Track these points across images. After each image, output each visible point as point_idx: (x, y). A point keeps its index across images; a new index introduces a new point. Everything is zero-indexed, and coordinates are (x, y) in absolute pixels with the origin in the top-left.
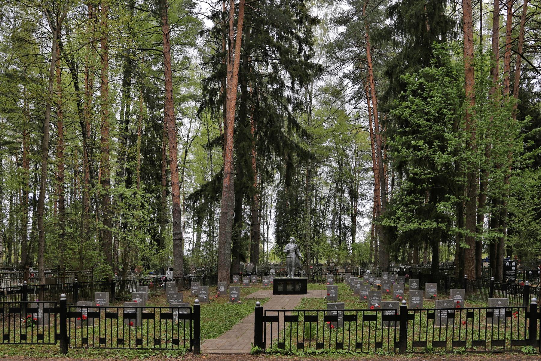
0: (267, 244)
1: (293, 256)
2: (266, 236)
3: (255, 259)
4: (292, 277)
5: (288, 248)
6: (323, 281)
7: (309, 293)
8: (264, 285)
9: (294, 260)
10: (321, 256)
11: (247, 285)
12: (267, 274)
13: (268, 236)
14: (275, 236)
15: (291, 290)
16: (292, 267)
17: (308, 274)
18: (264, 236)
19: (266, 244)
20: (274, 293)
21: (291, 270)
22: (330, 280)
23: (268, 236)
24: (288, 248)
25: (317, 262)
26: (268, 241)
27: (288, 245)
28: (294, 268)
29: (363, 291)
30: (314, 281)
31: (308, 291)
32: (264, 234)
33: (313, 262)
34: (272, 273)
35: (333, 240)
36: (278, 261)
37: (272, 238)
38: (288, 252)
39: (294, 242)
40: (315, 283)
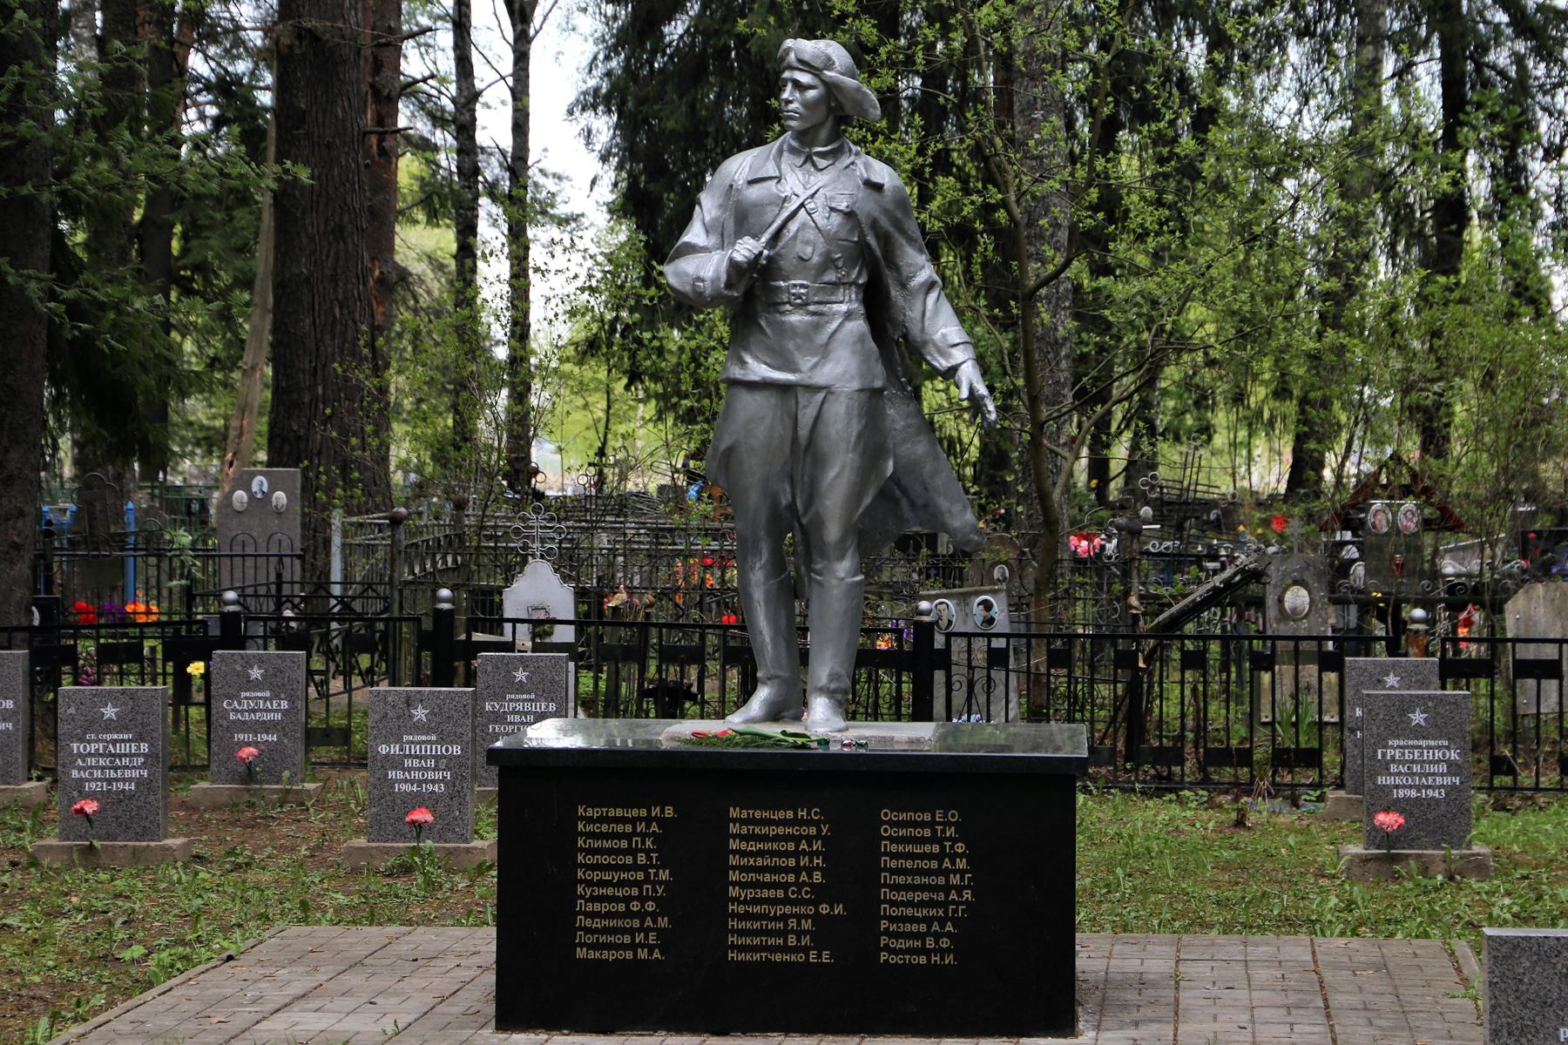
0: (517, 235)
1: (838, 361)
2: (493, 128)
3: (316, 424)
4: (822, 720)
5: (742, 219)
6: (1283, 758)
7: (1119, 999)
8: (389, 814)
9: (841, 423)
10: (1203, 401)
11: (128, 817)
12: (449, 648)
13: (520, 127)
14: (603, 126)
15: (797, 948)
16: (811, 546)
17: (1047, 660)
18: (464, 127)
19: (491, 229)
20: (510, 1016)
21: (792, 589)
22: (1422, 765)
23: (520, 127)
24: (742, 219)
25: (1139, 465)
26: (522, 209)
27: (740, 166)
28: (843, 571)
29: (1394, 749)
30: (1144, 755)
31: (1094, 954)
32: (469, 97)
33: (1099, 468)
34: (541, 626)
35: (1358, 174)
36: (653, 455)
37: (576, 163)
38: (753, 294)
39: (833, 125)
40: (1164, 787)
